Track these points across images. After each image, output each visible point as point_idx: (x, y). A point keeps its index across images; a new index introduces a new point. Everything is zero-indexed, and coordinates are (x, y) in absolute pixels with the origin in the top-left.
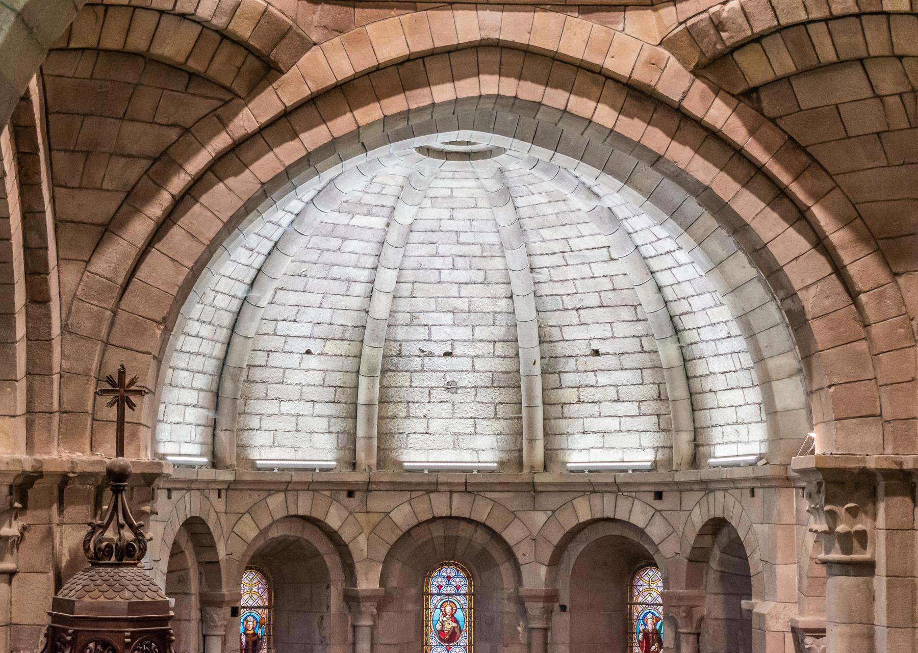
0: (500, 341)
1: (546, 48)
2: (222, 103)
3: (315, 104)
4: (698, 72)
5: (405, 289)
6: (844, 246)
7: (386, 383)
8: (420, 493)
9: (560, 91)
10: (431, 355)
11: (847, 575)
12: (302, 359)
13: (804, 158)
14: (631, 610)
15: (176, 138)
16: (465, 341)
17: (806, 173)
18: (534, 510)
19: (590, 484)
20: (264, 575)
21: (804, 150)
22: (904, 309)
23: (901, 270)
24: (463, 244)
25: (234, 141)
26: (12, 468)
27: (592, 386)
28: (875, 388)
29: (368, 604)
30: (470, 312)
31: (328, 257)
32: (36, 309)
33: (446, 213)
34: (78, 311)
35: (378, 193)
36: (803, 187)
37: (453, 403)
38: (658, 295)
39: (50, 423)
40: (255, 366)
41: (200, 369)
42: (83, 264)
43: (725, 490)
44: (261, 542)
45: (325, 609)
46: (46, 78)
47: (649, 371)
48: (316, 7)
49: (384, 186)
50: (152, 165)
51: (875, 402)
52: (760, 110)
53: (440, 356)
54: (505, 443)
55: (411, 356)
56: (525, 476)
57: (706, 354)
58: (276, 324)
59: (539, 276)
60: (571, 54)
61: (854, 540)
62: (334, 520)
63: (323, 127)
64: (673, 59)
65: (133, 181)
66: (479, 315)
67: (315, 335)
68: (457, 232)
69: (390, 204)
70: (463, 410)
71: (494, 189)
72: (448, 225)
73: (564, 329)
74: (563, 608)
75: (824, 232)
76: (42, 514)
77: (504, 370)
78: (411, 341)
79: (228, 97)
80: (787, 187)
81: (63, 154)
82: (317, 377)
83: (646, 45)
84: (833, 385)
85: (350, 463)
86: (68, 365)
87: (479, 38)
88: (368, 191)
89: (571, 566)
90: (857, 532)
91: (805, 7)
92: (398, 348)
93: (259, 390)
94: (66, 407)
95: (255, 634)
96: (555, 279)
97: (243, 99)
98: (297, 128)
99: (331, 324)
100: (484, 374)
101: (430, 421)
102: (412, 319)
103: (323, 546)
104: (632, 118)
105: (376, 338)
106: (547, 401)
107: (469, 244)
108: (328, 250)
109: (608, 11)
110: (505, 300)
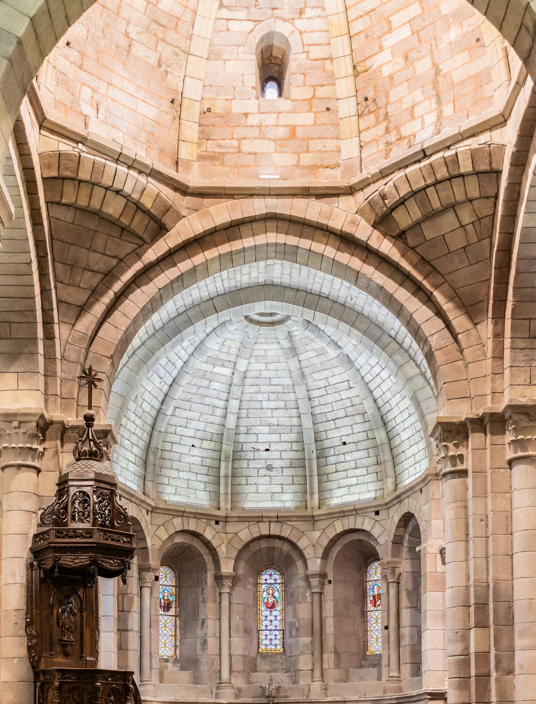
0: (294, 442)
2: (138, 246)
4: (375, 225)
5: (244, 413)
7: (235, 466)
8: (254, 523)
9: (307, 240)
10: (258, 450)
11: (454, 478)
12: (190, 449)
13: (429, 268)
14: (366, 585)
16: (276, 442)
17: (431, 275)
18: (314, 530)
19: (342, 512)
20: (173, 569)
21: (429, 263)
22: (480, 342)
23: (478, 321)
25: (145, 266)
26: (38, 412)
27: (343, 462)
28: (467, 384)
29: (227, 581)
30: (278, 425)
31: (202, 391)
33: (263, 366)
34: (69, 349)
36: (428, 282)
37: (270, 477)
41: (136, 443)
42: (71, 326)
43: (408, 497)
44: (169, 544)
45: (204, 584)
46: (51, 219)
47: (371, 449)
48: (184, 197)
49: (230, 348)
50: (104, 277)
52: (406, 244)
55: (248, 451)
56: (309, 512)
57: (399, 431)
58: (176, 428)
59: (314, 403)
60: (311, 219)
61: (458, 460)
62: (208, 535)
63: (189, 260)
64: (363, 220)
65: (95, 285)
66: (283, 427)
67: (197, 437)
68: (269, 378)
69: (234, 360)
70: (276, 480)
72: (265, 374)
73: (328, 432)
74: (330, 582)
75: (440, 304)
76: (52, 443)
79: (141, 243)
81: (60, 264)
82: (198, 460)
86: (65, 375)
87: (265, 212)
88: (222, 351)
90: (458, 455)
91: (424, 178)
92: (241, 447)
93: (168, 464)
94: (64, 396)
95: (168, 600)
96: (322, 404)
98: (176, 261)
99: (205, 431)
101: (259, 486)
102: (248, 430)
103: (203, 550)
104: (344, 253)
105: (229, 440)
106: (320, 473)
107: (276, 385)
108: (202, 387)
109: (330, 197)
110: (296, 418)
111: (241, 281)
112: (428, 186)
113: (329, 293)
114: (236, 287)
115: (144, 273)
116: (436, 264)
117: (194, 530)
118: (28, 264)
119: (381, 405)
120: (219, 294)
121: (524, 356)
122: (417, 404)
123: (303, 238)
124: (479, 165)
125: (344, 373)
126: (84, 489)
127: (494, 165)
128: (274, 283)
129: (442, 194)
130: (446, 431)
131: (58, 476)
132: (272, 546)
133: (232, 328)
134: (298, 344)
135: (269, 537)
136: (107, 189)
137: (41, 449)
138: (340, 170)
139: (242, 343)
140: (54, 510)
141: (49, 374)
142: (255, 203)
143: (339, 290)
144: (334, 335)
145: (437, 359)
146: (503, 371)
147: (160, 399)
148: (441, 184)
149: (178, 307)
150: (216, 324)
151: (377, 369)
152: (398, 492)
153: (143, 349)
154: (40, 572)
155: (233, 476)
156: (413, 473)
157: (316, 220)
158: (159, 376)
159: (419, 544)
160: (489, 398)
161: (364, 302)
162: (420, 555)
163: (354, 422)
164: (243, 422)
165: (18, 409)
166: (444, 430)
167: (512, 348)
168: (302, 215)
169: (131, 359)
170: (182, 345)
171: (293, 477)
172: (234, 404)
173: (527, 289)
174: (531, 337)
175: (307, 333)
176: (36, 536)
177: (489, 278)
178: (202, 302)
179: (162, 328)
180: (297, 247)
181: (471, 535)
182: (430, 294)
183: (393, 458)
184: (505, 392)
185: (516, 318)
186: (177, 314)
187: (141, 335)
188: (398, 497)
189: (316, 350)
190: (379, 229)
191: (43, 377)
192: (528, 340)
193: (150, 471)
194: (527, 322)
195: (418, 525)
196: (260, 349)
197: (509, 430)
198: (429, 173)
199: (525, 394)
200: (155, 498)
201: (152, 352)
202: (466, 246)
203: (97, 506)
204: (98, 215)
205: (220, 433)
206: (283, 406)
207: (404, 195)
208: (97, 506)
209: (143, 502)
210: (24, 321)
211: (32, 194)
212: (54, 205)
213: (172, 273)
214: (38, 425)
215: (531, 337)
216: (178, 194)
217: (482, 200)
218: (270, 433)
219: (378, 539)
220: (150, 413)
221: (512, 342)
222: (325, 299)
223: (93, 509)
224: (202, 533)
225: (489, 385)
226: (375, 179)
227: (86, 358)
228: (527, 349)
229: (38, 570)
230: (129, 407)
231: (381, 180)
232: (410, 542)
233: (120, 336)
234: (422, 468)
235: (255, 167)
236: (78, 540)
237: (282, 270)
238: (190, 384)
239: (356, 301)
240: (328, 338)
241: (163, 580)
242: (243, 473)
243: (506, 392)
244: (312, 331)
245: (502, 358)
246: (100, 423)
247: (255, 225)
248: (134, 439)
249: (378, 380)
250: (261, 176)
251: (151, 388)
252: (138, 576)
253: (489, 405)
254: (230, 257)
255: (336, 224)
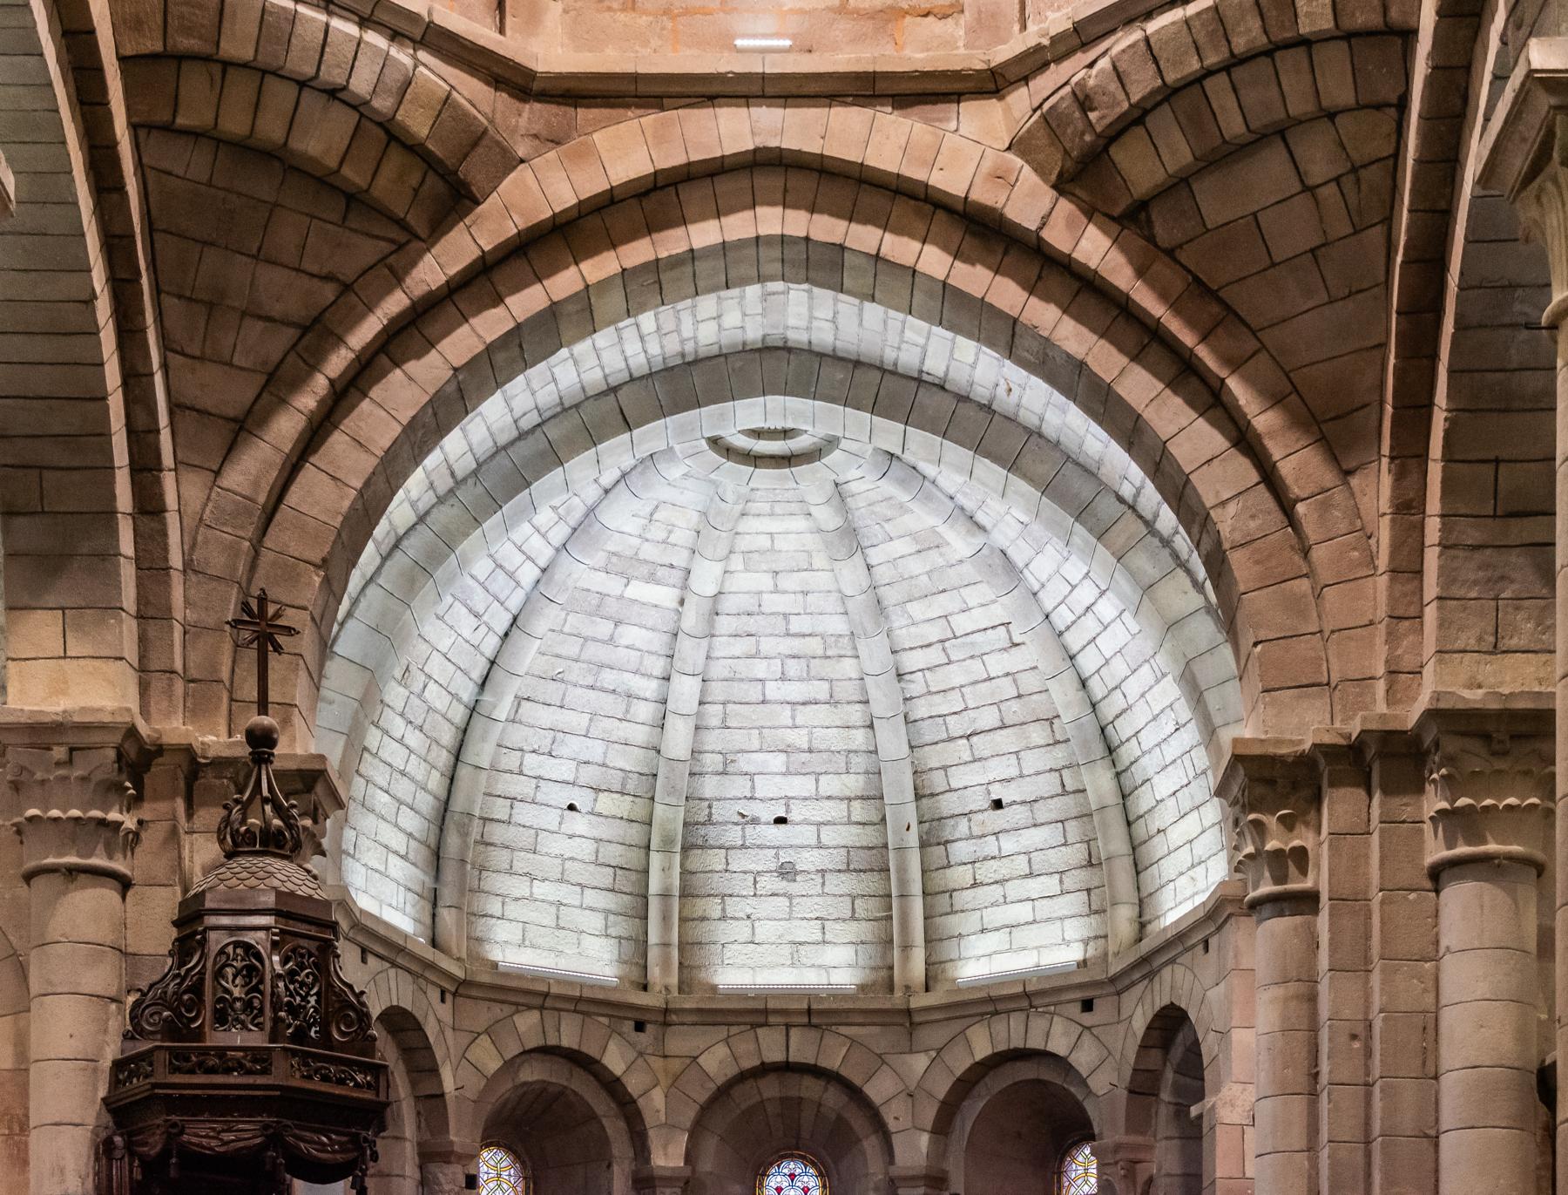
0: (857, 798)
1: (847, 158)
2: (394, 247)
3: (525, 254)
4: (1062, 186)
5: (714, 713)
6: (1271, 435)
8: (743, 1028)
10: (755, 821)
11: (1281, 915)
12: (562, 817)
13: (1215, 309)
15: (333, 298)
16: (805, 799)
17: (1220, 330)
18: (911, 1052)
22: (1358, 524)
23: (1354, 464)
24: (793, 635)
26: (119, 719)
30: (810, 751)
31: (595, 652)
32: (148, 523)
33: (765, 582)
35: (663, 542)
36: (1215, 350)
37: (790, 897)
38: (1081, 693)
39: (170, 685)
40: (492, 820)
41: (409, 801)
43: (1172, 961)
44: (505, 1087)
46: (148, 171)
50: (300, 339)
51: (1320, 666)
52: (1151, 239)
53: (768, 824)
54: (868, 955)
55: (726, 823)
57: (1151, 773)
58: (522, 757)
59: (912, 686)
60: (882, 167)
61: (1290, 863)
62: (615, 1060)
63: (538, 287)
64: (1027, 168)
65: (276, 357)
66: (825, 756)
67: (582, 781)
69: (684, 564)
71: (832, 527)
72: (773, 603)
75: (1245, 415)
76: (162, 807)
77: (865, 844)
78: (725, 799)
79: (403, 238)
80: (1191, 350)
82: (585, 849)
83: (988, 150)
84: (1261, 642)
85: (639, 984)
87: (751, 147)
88: (648, 536)
89: (966, 1136)
90: (1293, 849)
91: (1197, 49)
94: (194, 673)
96: (933, 689)
97: (423, 241)
98: (501, 289)
99: (604, 765)
100: (835, 852)
101: (757, 924)
102: (725, 764)
103: (600, 1104)
104: (973, 264)
105: (672, 791)
106: (929, 890)
107: (804, 636)
108: (595, 640)
109: (935, 103)
110: (862, 730)
111: (695, 338)
112: (1209, 73)
113: (946, 374)
114: (683, 355)
115: (412, 323)
116: (1230, 295)
117: (575, 1047)
118: (85, 302)
119: (1099, 697)
120: (636, 374)
121: (1480, 568)
122: (1196, 697)
123: (860, 222)
124: (1353, 15)
125: (994, 602)
126: (250, 938)
127: (1394, 14)
128: (790, 344)
129: (1250, 97)
130: (1257, 780)
131: (179, 898)
132: (793, 1093)
133: (675, 472)
134: (862, 518)
135: (786, 1068)
136: (302, 84)
137: (130, 822)
138: (962, 22)
139: (704, 514)
140: (165, 993)
141: (152, 613)
142: (721, 121)
143: (973, 366)
144: (965, 494)
145: (1237, 574)
146: (1422, 611)
147: (477, 675)
148: (1246, 66)
149: (517, 413)
150: (627, 462)
151: (1086, 594)
152: (1146, 946)
153: (423, 536)
154: (131, 1165)
155: (686, 894)
156: (1188, 893)
157: (892, 167)
158: (470, 611)
159: (1199, 1096)
160: (1381, 687)
161: (1044, 401)
162: (1200, 1127)
163: (1023, 745)
164: (712, 740)
165: (65, 712)
166: (1253, 779)
167: (1445, 546)
168: (853, 155)
169: (388, 563)
170: (535, 521)
171: (853, 898)
172: (685, 691)
173: (1489, 376)
174: (1499, 513)
175: (888, 487)
176: (118, 1065)
177: (1383, 340)
178: (587, 398)
179: (475, 473)
180: (842, 248)
181: (1324, 1079)
182: (1219, 383)
183: (1134, 849)
184: (1425, 671)
185: (1457, 457)
186: (515, 434)
187: (414, 494)
188: (1145, 960)
189: (913, 536)
190: (1074, 195)
191: (134, 623)
192: (1490, 520)
193: (450, 878)
194: (1488, 470)
195: (1196, 1043)
196: (756, 531)
197: (1434, 781)
198: (1211, 35)
199: (1480, 678)
200: (464, 956)
201: (448, 543)
202: (1318, 247)
203: (281, 984)
204: (279, 159)
205: (645, 770)
206: (824, 696)
207: (1143, 99)
208: (281, 984)
209: (431, 966)
210: (76, 463)
211: (91, 104)
212: (154, 133)
213: (491, 324)
214: (120, 756)
215: (1499, 513)
216: (504, 95)
217: (1362, 113)
218: (787, 773)
219: (1089, 1081)
220: (449, 715)
221: (1445, 529)
222: (935, 389)
223: (273, 994)
224: (597, 1057)
225: (1382, 651)
226: (1062, 49)
227: (253, 567)
228: (1487, 547)
229: (126, 1159)
230: (387, 699)
231: (1079, 55)
232: (1177, 1090)
233: (346, 504)
234: (1211, 880)
235: (721, 15)
236: (235, 1078)
237: (811, 309)
238: (561, 632)
239: (1020, 398)
240: (947, 500)
241: (492, 1185)
242: (714, 886)
243: (1428, 672)
244: (902, 482)
245: (1419, 573)
246: (294, 747)
247: (724, 185)
248: (403, 788)
249: (1090, 625)
250: (739, 43)
251: (449, 642)
252: (417, 1176)
253: (1381, 707)
254: (652, 279)
255: (951, 180)
